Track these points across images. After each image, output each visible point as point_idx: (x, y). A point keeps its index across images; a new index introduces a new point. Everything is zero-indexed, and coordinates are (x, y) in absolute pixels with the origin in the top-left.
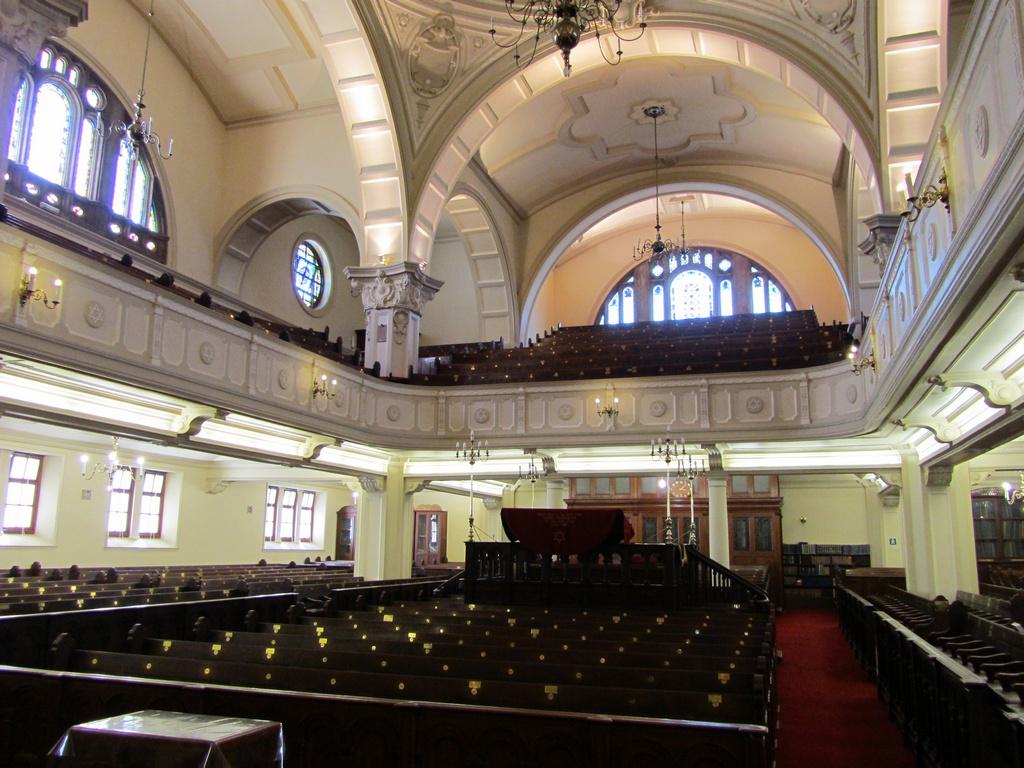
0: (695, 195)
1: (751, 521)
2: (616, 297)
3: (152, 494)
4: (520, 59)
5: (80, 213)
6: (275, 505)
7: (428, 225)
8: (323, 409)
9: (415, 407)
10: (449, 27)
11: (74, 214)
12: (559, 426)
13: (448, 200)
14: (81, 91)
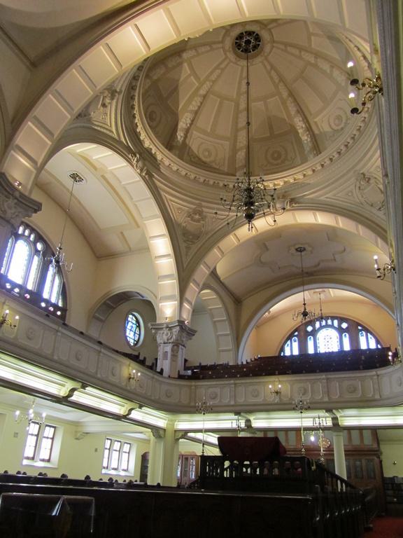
0: (326, 290)
1: (364, 461)
2: (289, 342)
3: (47, 438)
4: (232, 227)
5: (28, 297)
6: (109, 449)
7: (190, 303)
8: (133, 388)
9: (181, 391)
10: (200, 213)
11: (26, 298)
12: (252, 400)
13: (199, 292)
14: (35, 243)
